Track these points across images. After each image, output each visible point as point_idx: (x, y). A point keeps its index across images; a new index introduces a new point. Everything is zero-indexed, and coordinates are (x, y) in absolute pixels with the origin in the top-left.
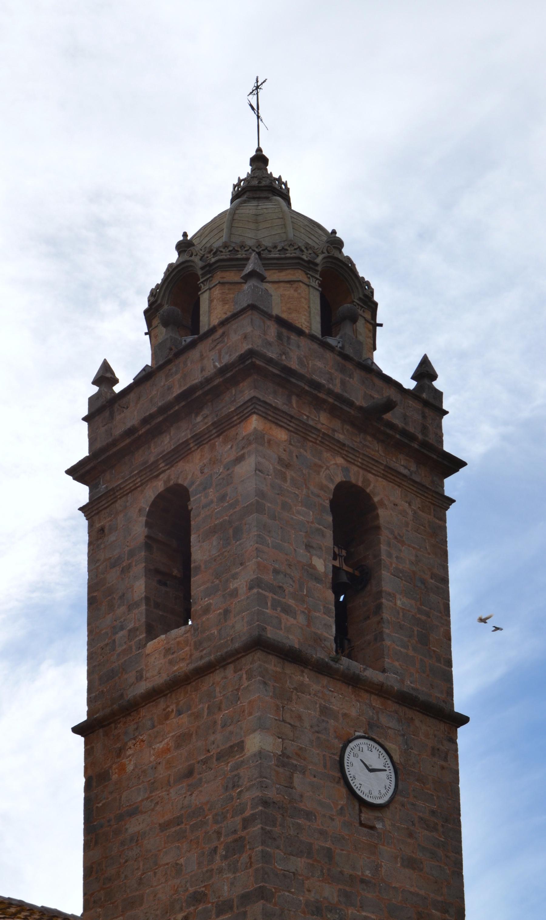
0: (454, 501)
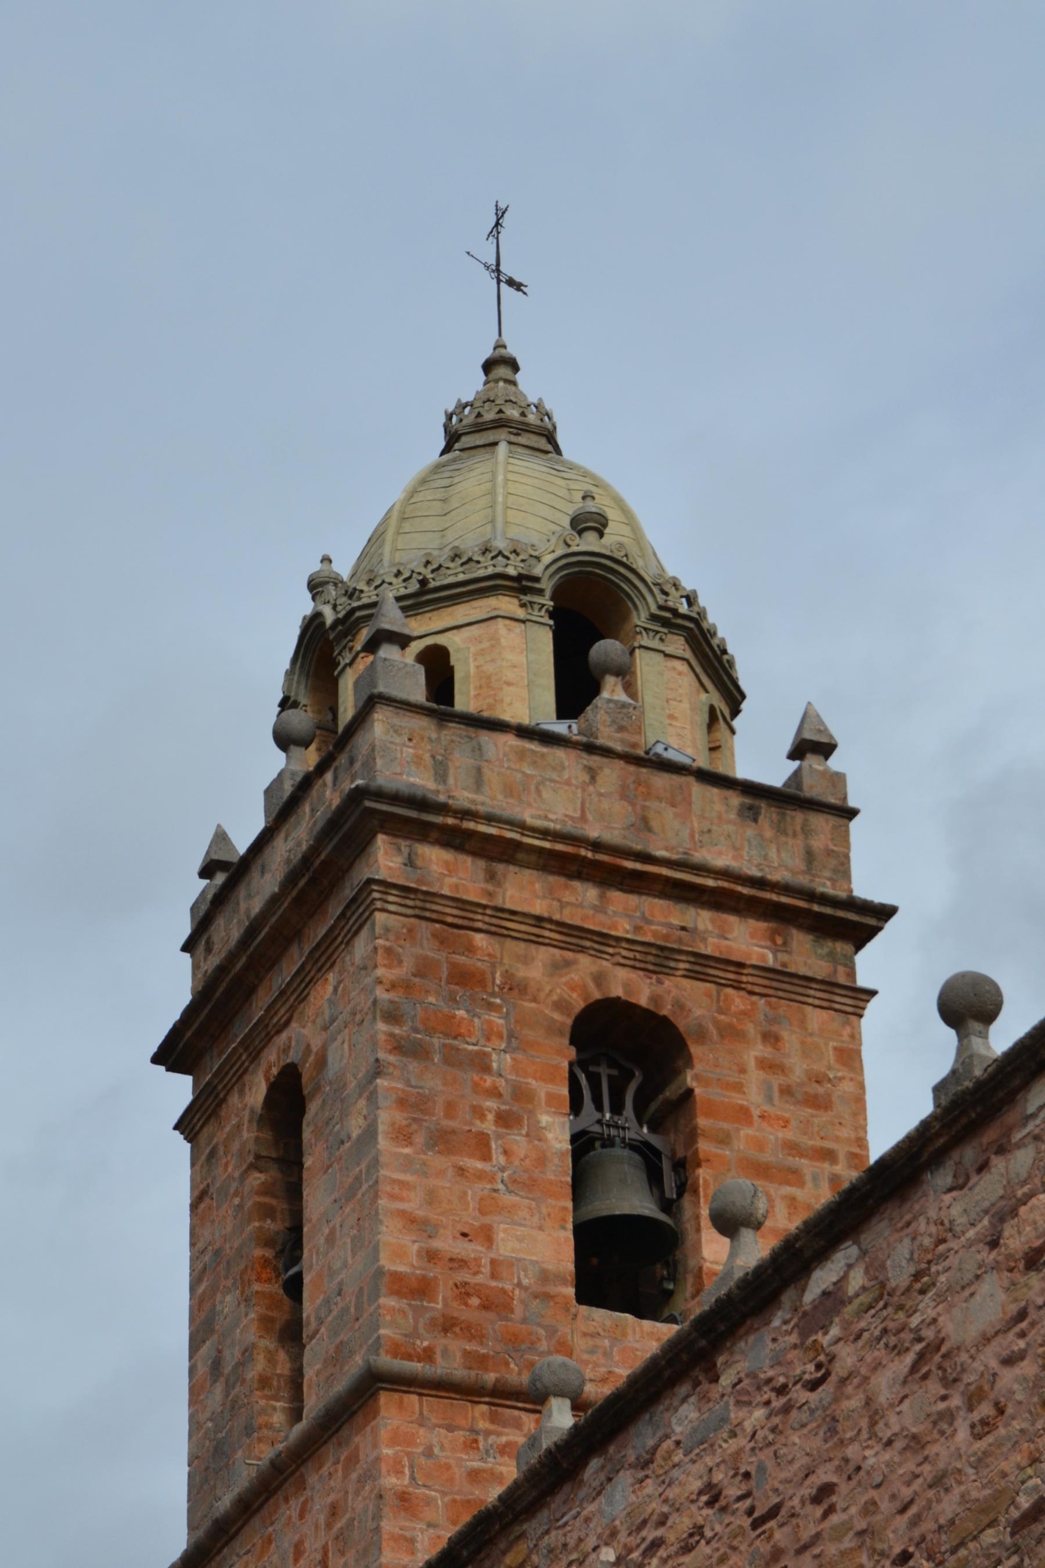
0: (873, 993)
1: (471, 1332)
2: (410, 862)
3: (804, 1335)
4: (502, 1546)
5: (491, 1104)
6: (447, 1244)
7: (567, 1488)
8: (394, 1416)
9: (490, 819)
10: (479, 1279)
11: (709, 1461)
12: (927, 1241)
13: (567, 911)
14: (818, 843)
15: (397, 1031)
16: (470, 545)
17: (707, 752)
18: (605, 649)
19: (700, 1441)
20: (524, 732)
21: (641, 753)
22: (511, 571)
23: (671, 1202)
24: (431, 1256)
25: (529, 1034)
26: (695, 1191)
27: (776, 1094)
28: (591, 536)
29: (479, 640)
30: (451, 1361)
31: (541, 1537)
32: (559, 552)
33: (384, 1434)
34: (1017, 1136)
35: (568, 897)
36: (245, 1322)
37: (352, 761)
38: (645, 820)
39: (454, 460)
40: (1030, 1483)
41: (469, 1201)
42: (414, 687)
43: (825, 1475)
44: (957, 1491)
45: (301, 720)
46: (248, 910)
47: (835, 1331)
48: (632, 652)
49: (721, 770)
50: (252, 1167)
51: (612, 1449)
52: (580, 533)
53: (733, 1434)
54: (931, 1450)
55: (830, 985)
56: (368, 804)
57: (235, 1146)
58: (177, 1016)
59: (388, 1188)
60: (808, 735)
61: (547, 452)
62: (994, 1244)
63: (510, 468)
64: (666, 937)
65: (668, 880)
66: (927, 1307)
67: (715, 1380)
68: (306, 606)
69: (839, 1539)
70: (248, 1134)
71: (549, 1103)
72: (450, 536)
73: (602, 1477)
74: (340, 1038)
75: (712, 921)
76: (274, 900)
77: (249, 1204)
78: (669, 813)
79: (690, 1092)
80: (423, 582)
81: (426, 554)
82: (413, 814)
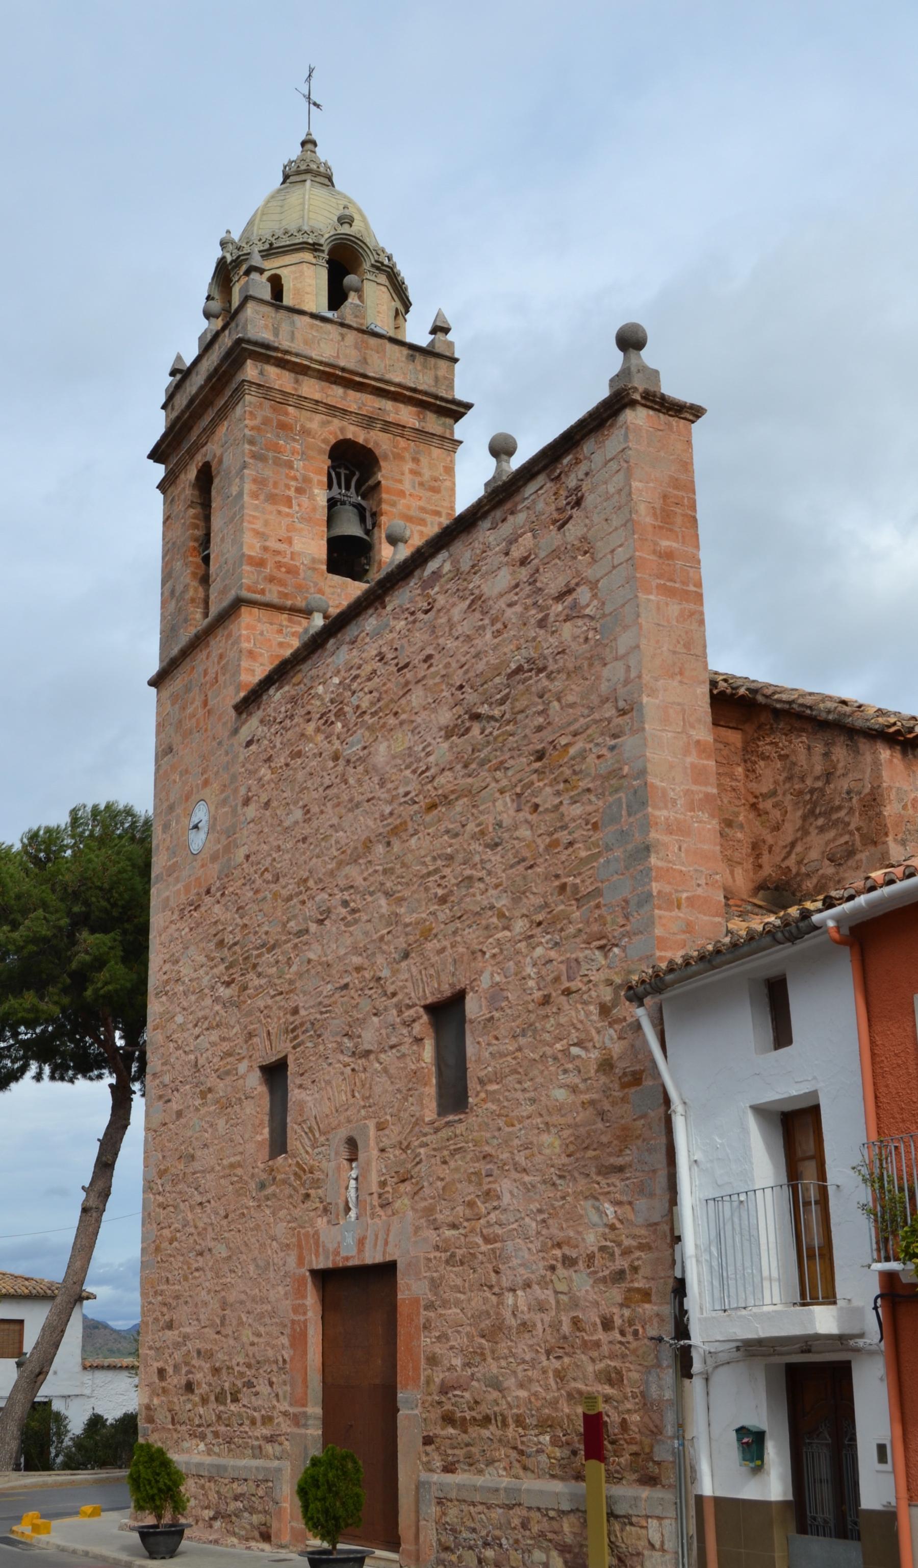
0: (461, 442)
1: (282, 583)
2: (261, 373)
5: (293, 483)
6: (273, 544)
7: (320, 651)
8: (247, 616)
9: (297, 355)
10: (285, 560)
11: (381, 642)
12: (478, 552)
14: (441, 373)
16: (292, 228)
18: (350, 279)
20: (313, 316)
22: (310, 241)
24: (265, 549)
25: (311, 453)
26: (380, 527)
28: (346, 226)
30: (272, 596)
33: (243, 625)
34: (520, 507)
35: (330, 392)
37: (237, 326)
38: (365, 359)
41: (281, 525)
42: (266, 293)
43: (429, 651)
44: (485, 660)
47: (436, 589)
49: (399, 337)
50: (190, 506)
51: (339, 635)
53: (391, 631)
55: (443, 438)
57: (183, 497)
60: (439, 324)
62: (507, 554)
65: (374, 387)
66: (476, 580)
67: (384, 607)
68: (219, 253)
69: (434, 678)
70: (188, 492)
72: (284, 223)
76: (202, 388)
78: (376, 356)
79: (379, 482)
80: (271, 244)
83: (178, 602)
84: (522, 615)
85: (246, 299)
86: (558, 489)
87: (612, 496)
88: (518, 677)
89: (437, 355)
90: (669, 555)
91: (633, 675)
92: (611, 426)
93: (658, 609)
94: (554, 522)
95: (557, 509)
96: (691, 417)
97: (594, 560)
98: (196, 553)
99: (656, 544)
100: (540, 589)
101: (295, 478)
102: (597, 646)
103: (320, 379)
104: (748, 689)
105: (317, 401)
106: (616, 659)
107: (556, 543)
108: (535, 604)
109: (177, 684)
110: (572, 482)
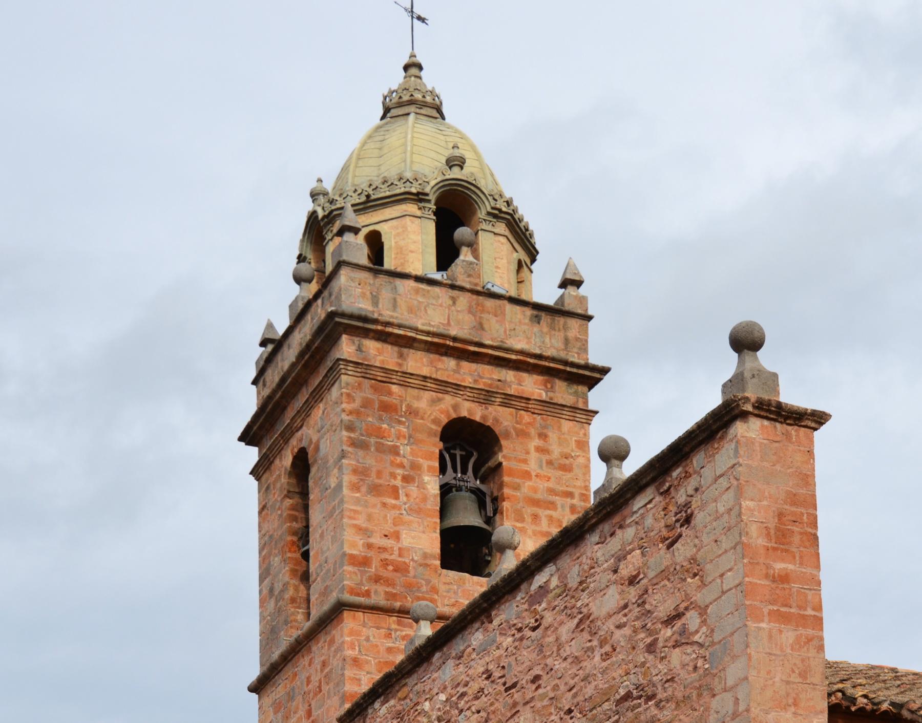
0: (596, 412)
1: (389, 582)
2: (359, 349)
3: (531, 605)
4: (397, 688)
5: (400, 471)
6: (377, 540)
7: (425, 665)
8: (350, 621)
9: (400, 326)
10: (393, 557)
11: (487, 659)
12: (586, 567)
13: (439, 373)
14: (571, 334)
15: (352, 435)
16: (392, 174)
17: (516, 284)
18: (462, 233)
19: (483, 650)
20: (418, 279)
21: (479, 288)
22: (414, 190)
23: (490, 518)
24: (369, 546)
25: (419, 436)
26: (502, 513)
27: (544, 465)
28: (456, 169)
29: (397, 228)
30: (378, 598)
31: (413, 686)
32: (439, 179)
33: (346, 631)
34: (628, 521)
35: (440, 365)
36: (284, 571)
37: (330, 295)
38: (481, 325)
39: (387, 124)
40: (625, 683)
41: (388, 518)
42: (362, 256)
43: (537, 671)
44: (594, 683)
45: (307, 269)
46: (282, 367)
47: (544, 605)
48: (476, 234)
49: (524, 297)
50: (287, 496)
51: (445, 649)
52: (450, 168)
53: (498, 648)
54: (584, 664)
55: (574, 409)
56: (337, 319)
57: (278, 485)
58: (249, 419)
59: (348, 513)
60: (569, 276)
61: (436, 118)
62: (615, 571)
63: (415, 130)
64: (490, 386)
65: (491, 356)
66: (585, 598)
67: (491, 622)
68: (309, 206)
69: (542, 700)
70: (284, 480)
71: (429, 471)
72: (383, 168)
73: (441, 661)
74: (325, 437)
75: (515, 377)
76: (293, 365)
77: (285, 514)
78: (493, 320)
79: (500, 464)
80: (368, 196)
81: (370, 180)
82: (360, 324)
83: (277, 602)
84: (630, 639)
85: (339, 265)
86: (667, 504)
87: (722, 515)
88: (627, 704)
89: (564, 314)
90: (784, 578)
91: (741, 708)
92: (722, 438)
93: (770, 637)
94: (664, 539)
95: (667, 526)
96: (813, 425)
97: (704, 584)
98: (295, 548)
99: (768, 567)
100: (649, 611)
101: (401, 466)
102: (705, 675)
103: (428, 351)
104: (893, 704)
105: (425, 377)
106: (725, 690)
107: (666, 563)
108: (644, 626)
109: (278, 690)
110: (681, 498)
